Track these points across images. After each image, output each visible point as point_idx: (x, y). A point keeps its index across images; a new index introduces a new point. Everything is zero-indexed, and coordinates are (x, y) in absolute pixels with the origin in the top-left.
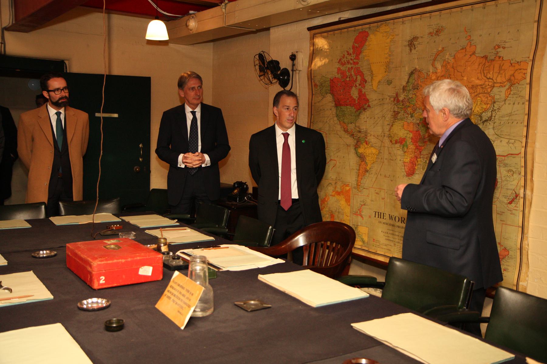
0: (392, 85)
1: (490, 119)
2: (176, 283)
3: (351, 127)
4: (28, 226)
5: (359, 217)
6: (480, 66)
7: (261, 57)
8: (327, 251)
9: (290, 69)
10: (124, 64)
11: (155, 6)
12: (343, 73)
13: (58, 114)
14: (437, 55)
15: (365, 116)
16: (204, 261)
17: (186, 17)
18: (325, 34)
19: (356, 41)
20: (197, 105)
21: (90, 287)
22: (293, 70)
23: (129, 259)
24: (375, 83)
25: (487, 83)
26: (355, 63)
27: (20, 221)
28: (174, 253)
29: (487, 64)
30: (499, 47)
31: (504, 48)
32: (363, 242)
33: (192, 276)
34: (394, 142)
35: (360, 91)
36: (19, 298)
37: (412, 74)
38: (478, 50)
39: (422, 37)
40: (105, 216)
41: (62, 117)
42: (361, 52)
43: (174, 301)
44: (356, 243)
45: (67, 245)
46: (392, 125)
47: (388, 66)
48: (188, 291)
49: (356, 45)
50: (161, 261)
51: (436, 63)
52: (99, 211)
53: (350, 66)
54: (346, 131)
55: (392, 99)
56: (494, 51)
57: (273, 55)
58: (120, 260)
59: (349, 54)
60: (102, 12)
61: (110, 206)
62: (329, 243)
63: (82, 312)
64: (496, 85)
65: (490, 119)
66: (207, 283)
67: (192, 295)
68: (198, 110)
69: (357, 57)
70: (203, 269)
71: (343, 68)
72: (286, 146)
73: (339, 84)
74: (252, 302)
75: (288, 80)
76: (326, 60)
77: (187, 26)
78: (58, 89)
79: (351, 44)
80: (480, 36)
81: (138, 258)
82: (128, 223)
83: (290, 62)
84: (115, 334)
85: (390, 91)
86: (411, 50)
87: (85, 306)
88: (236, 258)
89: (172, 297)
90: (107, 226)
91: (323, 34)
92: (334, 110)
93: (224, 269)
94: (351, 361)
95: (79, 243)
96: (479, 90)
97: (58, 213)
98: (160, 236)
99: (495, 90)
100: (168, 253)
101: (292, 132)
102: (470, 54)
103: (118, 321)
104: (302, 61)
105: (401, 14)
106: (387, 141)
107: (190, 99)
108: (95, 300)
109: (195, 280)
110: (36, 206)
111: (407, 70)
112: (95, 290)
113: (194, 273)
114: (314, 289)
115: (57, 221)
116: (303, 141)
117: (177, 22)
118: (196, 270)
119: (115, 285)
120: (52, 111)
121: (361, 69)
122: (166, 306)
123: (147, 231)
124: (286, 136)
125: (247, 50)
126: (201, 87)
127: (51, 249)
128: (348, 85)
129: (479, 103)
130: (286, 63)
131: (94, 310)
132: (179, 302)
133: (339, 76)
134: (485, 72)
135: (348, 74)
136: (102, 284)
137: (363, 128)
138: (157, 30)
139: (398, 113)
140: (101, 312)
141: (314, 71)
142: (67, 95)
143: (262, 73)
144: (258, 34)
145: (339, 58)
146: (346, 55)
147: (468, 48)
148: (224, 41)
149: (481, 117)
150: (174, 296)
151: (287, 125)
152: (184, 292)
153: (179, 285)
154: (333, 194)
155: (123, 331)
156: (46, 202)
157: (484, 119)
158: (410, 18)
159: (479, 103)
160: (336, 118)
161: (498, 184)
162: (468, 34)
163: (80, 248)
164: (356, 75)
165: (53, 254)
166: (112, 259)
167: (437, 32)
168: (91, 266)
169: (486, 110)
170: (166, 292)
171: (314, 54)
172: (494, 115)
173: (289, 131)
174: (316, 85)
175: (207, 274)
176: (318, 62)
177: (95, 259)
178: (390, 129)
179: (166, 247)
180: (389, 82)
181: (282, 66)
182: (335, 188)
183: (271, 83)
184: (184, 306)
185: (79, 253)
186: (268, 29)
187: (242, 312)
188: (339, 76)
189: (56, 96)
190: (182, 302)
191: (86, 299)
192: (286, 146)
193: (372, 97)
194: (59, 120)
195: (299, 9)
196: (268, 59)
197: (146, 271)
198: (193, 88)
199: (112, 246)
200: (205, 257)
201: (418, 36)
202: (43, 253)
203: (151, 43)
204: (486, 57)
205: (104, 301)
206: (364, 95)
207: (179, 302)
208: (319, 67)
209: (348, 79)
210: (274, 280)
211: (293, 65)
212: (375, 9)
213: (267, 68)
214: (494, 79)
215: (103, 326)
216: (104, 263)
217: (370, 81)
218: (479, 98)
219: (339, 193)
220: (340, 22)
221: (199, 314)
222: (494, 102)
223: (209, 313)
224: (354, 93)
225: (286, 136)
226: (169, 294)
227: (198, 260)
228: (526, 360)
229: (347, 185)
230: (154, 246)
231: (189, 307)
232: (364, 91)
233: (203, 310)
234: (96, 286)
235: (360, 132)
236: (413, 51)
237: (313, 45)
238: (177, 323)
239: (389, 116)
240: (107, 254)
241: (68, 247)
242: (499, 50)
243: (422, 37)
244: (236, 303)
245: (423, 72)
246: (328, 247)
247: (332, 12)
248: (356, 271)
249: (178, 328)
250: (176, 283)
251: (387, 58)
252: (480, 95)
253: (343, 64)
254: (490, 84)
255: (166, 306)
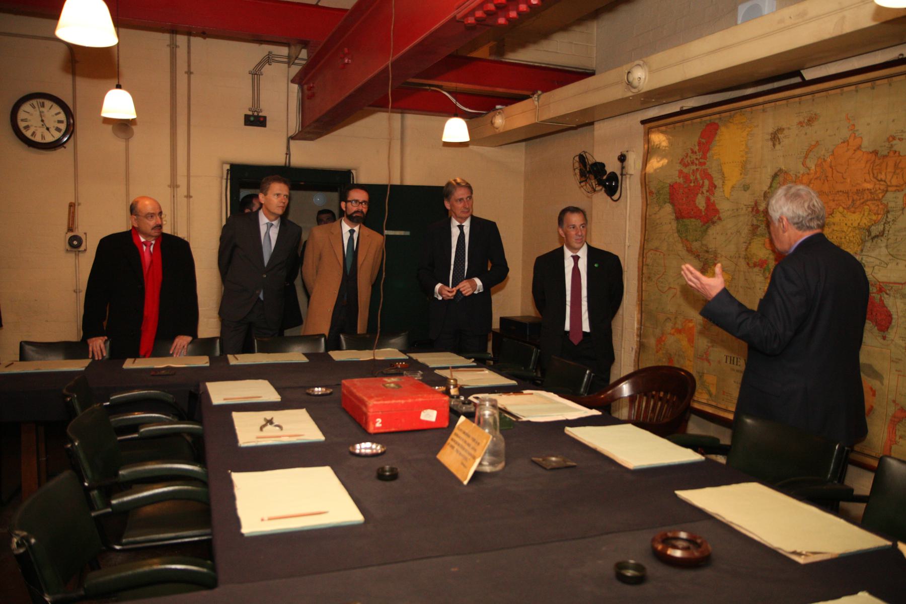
0: (749, 192)
1: (882, 234)
2: (461, 430)
3: (696, 245)
4: (305, 360)
5: (706, 364)
6: (868, 165)
7: (582, 159)
8: (659, 404)
9: (618, 173)
10: (417, 173)
11: (454, 100)
12: (686, 177)
13: (352, 232)
14: (810, 151)
15: (713, 231)
16: (494, 405)
17: (492, 113)
18: (663, 128)
19: (702, 136)
20: (465, 219)
21: (365, 431)
22: (622, 175)
23: (410, 401)
24: (727, 189)
25: (877, 186)
26: (702, 164)
27: (296, 355)
28: (466, 398)
29: (878, 162)
30: (894, 138)
31: (901, 140)
32: (710, 394)
33: (481, 423)
34: (752, 265)
35: (708, 199)
36: (290, 436)
37: (775, 176)
38: (865, 143)
39: (789, 129)
40: (389, 353)
41: (355, 236)
42: (708, 150)
43: (457, 451)
44: (696, 394)
45: (343, 381)
46: (750, 243)
47: (744, 167)
48: (474, 440)
49: (704, 141)
50: (446, 405)
51: (808, 161)
52: (380, 346)
53: (694, 167)
54: (690, 251)
55: (750, 209)
56: (887, 144)
57: (598, 155)
58: (399, 401)
59: (693, 152)
60: (387, 112)
61: (399, 340)
62: (662, 394)
63: (354, 458)
64: (890, 189)
65: (882, 234)
66: (498, 433)
67: (479, 444)
68: (467, 225)
69: (704, 156)
70: (492, 415)
71: (685, 170)
72: (576, 271)
73: (681, 191)
74: (554, 459)
75: (616, 187)
76: (665, 161)
77: (492, 123)
78: (356, 201)
79: (695, 139)
80: (868, 124)
81: (420, 400)
82: (416, 361)
83: (618, 164)
84: (388, 484)
85: (747, 199)
86: (774, 145)
87: (358, 451)
88: (541, 406)
89: (456, 447)
90: (391, 363)
91: (661, 128)
92: (674, 224)
93: (524, 419)
94: (666, 534)
95: (357, 381)
96: (867, 196)
97: (338, 347)
98: (449, 377)
99: (890, 196)
100: (458, 397)
101: (583, 253)
102: (855, 148)
103: (392, 470)
104: (634, 163)
105: (761, 99)
106: (742, 263)
107: (458, 212)
108: (368, 444)
109: (483, 427)
110: (314, 339)
111: (769, 171)
112: (370, 434)
113: (482, 420)
114: (635, 448)
115: (338, 356)
116: (596, 265)
117: (481, 119)
118: (484, 415)
119: (393, 429)
120: (346, 228)
121: (709, 171)
122: (449, 457)
123: (437, 372)
124: (576, 259)
125: (565, 151)
126: (470, 197)
127: (326, 387)
128: (693, 192)
129: (866, 214)
130: (612, 166)
131: (366, 456)
132: (463, 452)
133: (681, 181)
134: (875, 172)
135: (692, 177)
136: (379, 428)
137: (711, 246)
138: (456, 130)
139: (757, 227)
140: (374, 459)
141: (649, 174)
142: (365, 210)
143: (583, 179)
144: (579, 130)
145: (680, 157)
146: (690, 154)
147: (851, 141)
148: (538, 140)
149: (869, 231)
150: (459, 445)
151: (577, 245)
152: (469, 441)
153: (464, 433)
154: (673, 331)
155: (398, 481)
156: (327, 334)
157: (873, 234)
158: (773, 104)
159: (866, 214)
160: (676, 235)
161: (894, 321)
162: (852, 122)
163: (357, 385)
164: (703, 179)
165: (328, 392)
166: (391, 399)
167: (809, 121)
168: (366, 406)
169: (876, 223)
170: (449, 441)
171: (648, 154)
172: (887, 229)
173: (579, 254)
174: (651, 193)
175: (498, 420)
176: (655, 164)
177: (371, 398)
178: (747, 249)
179: (456, 389)
180: (746, 188)
181: (609, 170)
182: (675, 324)
183: (595, 191)
184: (469, 457)
185: (355, 391)
186: (592, 124)
187: (539, 470)
188: (681, 181)
189: (352, 208)
190: (467, 454)
191: (360, 443)
192: (576, 271)
193: (724, 206)
194: (351, 239)
195: (627, 98)
196: (591, 161)
197: (430, 416)
198: (461, 200)
199: (392, 385)
200: (495, 401)
201: (784, 127)
202: (318, 390)
203: (447, 144)
204: (875, 153)
205: (379, 447)
206: (714, 204)
207: (463, 452)
208: (655, 170)
209: (692, 184)
210: (588, 435)
211: (623, 168)
212: (730, 93)
213: (590, 172)
214: (887, 181)
215: (375, 474)
216: (382, 404)
217: (720, 185)
218: (866, 207)
219: (679, 331)
220: (682, 112)
221: (487, 469)
222: (888, 212)
223: (499, 467)
224: (701, 202)
225: (576, 259)
226: (452, 443)
227: (487, 404)
228: (278, 389)
229: (691, 321)
230: (443, 388)
231: (474, 458)
232: (712, 199)
233: (492, 464)
234: (371, 430)
235: (707, 252)
236: (778, 147)
237: (648, 141)
238: (459, 476)
239: (746, 231)
240: (386, 394)
241: (344, 385)
242: (894, 142)
243: (789, 129)
244: (534, 459)
245: (791, 173)
246: (660, 399)
247: (670, 100)
248: (695, 428)
249: (461, 483)
250: (461, 430)
251: (742, 156)
252: (869, 203)
253: (686, 165)
254: (882, 187)
255: (449, 457)
